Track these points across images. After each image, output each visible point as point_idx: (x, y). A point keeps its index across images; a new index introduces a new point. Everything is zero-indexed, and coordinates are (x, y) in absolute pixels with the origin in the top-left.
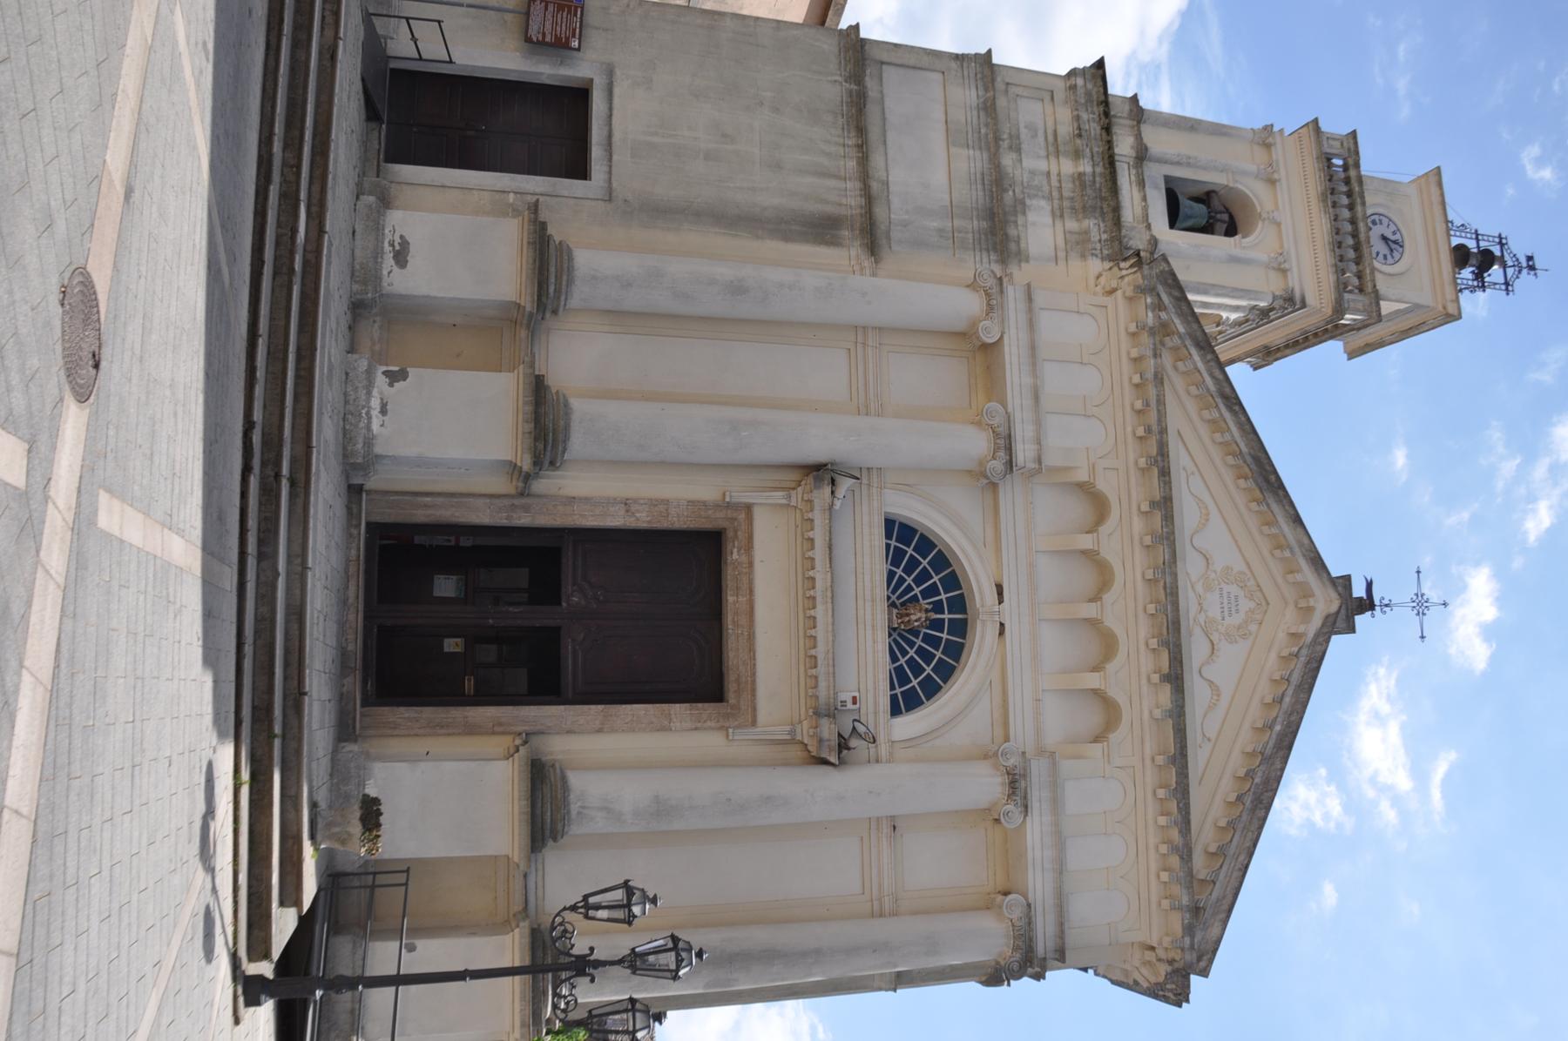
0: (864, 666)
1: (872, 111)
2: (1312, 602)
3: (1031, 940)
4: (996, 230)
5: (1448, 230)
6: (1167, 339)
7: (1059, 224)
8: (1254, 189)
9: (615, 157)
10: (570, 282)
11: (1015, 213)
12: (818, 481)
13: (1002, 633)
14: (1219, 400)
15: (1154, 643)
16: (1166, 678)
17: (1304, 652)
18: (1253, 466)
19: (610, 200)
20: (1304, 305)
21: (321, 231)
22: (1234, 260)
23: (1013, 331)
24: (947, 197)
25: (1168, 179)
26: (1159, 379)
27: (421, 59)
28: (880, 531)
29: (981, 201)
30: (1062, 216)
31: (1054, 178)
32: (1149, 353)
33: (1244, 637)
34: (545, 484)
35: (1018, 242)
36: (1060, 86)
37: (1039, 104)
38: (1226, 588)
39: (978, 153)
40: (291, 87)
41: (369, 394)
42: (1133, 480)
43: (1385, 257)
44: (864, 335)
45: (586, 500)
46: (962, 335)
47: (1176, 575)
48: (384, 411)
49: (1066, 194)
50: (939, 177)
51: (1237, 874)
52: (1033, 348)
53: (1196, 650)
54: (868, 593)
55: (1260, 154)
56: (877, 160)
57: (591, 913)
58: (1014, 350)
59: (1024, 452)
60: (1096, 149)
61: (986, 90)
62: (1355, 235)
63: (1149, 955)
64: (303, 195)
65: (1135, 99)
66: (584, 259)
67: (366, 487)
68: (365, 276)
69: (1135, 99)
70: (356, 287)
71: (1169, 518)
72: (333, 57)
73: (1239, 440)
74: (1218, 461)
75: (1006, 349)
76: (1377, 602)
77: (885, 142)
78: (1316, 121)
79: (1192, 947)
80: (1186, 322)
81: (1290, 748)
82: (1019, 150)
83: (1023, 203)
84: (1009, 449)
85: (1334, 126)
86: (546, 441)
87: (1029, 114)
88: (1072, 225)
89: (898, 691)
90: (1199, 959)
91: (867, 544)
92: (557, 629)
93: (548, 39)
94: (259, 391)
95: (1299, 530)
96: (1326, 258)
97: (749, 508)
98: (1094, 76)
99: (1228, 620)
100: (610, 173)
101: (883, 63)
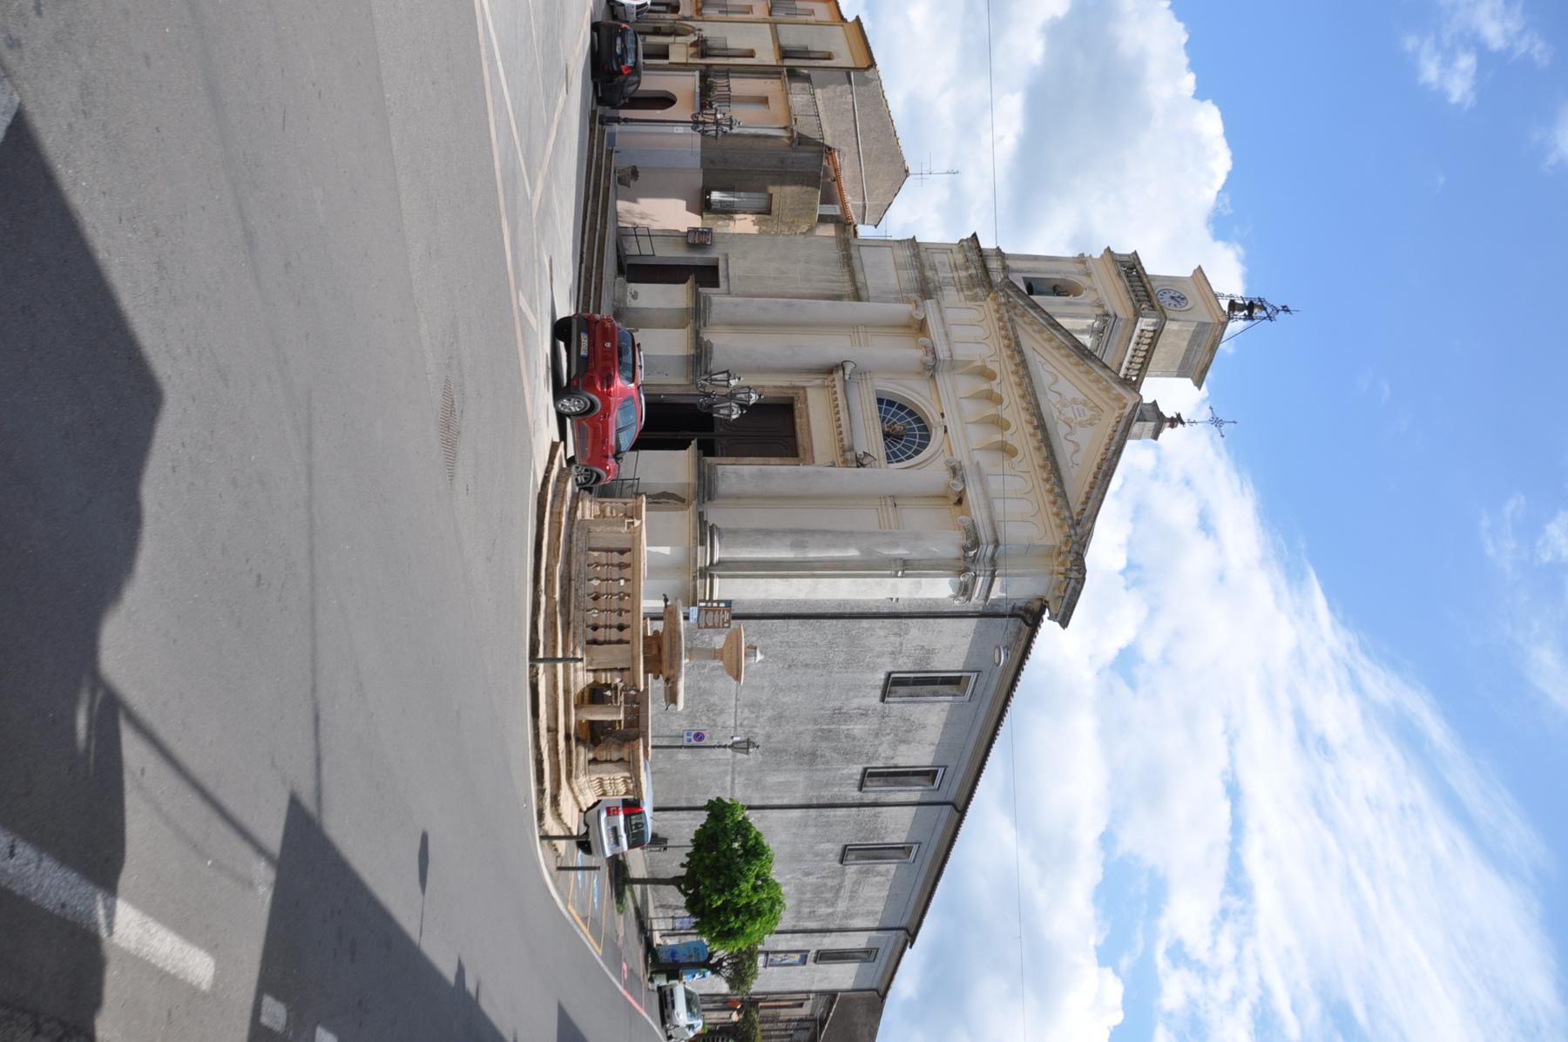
1: (856, 262)
8: (1083, 281)
16: (1047, 458)
22: (1070, 304)
26: (1011, 320)
28: (875, 405)
36: (955, 249)
44: (895, 500)
46: (907, 326)
50: (893, 281)
53: (1059, 431)
55: (1081, 267)
56: (860, 277)
59: (943, 354)
69: (1122, 573)
85: (1123, 248)
87: (938, 258)
96: (1124, 297)
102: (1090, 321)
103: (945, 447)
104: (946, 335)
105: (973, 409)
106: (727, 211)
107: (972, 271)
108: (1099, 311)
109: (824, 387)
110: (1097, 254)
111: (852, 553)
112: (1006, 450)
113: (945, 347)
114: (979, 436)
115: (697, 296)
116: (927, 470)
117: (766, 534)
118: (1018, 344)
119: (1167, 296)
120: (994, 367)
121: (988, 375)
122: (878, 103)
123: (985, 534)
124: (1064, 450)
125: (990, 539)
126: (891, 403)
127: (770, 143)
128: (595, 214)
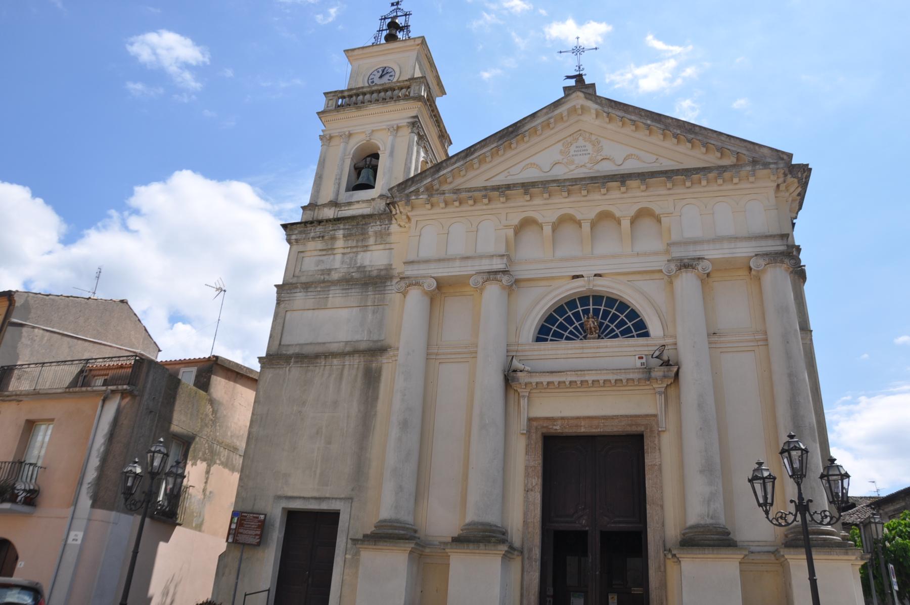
0: (621, 353)
1: (307, 350)
3: (776, 253)
4: (374, 282)
7: (370, 248)
8: (354, 144)
9: (327, 495)
10: (397, 521)
12: (515, 379)
13: (600, 275)
14: (468, 159)
19: (352, 499)
20: (416, 117)
22: (392, 154)
25: (348, 190)
26: (456, 191)
28: (542, 345)
30: (367, 246)
31: (346, 251)
32: (442, 197)
33: (599, 143)
36: (296, 248)
38: (572, 153)
39: (331, 292)
42: (512, 205)
45: (525, 514)
46: (432, 300)
49: (354, 244)
50: (344, 313)
51: (732, 141)
52: (440, 260)
53: (607, 168)
55: (334, 142)
56: (334, 348)
58: (441, 270)
59: (498, 264)
61: (296, 288)
66: (385, 513)
69: (304, 208)
71: (533, 184)
73: (490, 148)
75: (440, 275)
77: (324, 343)
78: (318, 113)
79: (775, 163)
80: (426, 177)
84: (496, 272)
86: (490, 536)
87: (310, 265)
88: (371, 241)
90: (783, 159)
93: (259, 533)
95: (539, 114)
97: (530, 420)
98: (291, 230)
100: (336, 499)
104: (467, 258)
107: (340, 234)
120: (515, 220)
122: (47, 301)
125: (779, 242)
127: (125, 421)
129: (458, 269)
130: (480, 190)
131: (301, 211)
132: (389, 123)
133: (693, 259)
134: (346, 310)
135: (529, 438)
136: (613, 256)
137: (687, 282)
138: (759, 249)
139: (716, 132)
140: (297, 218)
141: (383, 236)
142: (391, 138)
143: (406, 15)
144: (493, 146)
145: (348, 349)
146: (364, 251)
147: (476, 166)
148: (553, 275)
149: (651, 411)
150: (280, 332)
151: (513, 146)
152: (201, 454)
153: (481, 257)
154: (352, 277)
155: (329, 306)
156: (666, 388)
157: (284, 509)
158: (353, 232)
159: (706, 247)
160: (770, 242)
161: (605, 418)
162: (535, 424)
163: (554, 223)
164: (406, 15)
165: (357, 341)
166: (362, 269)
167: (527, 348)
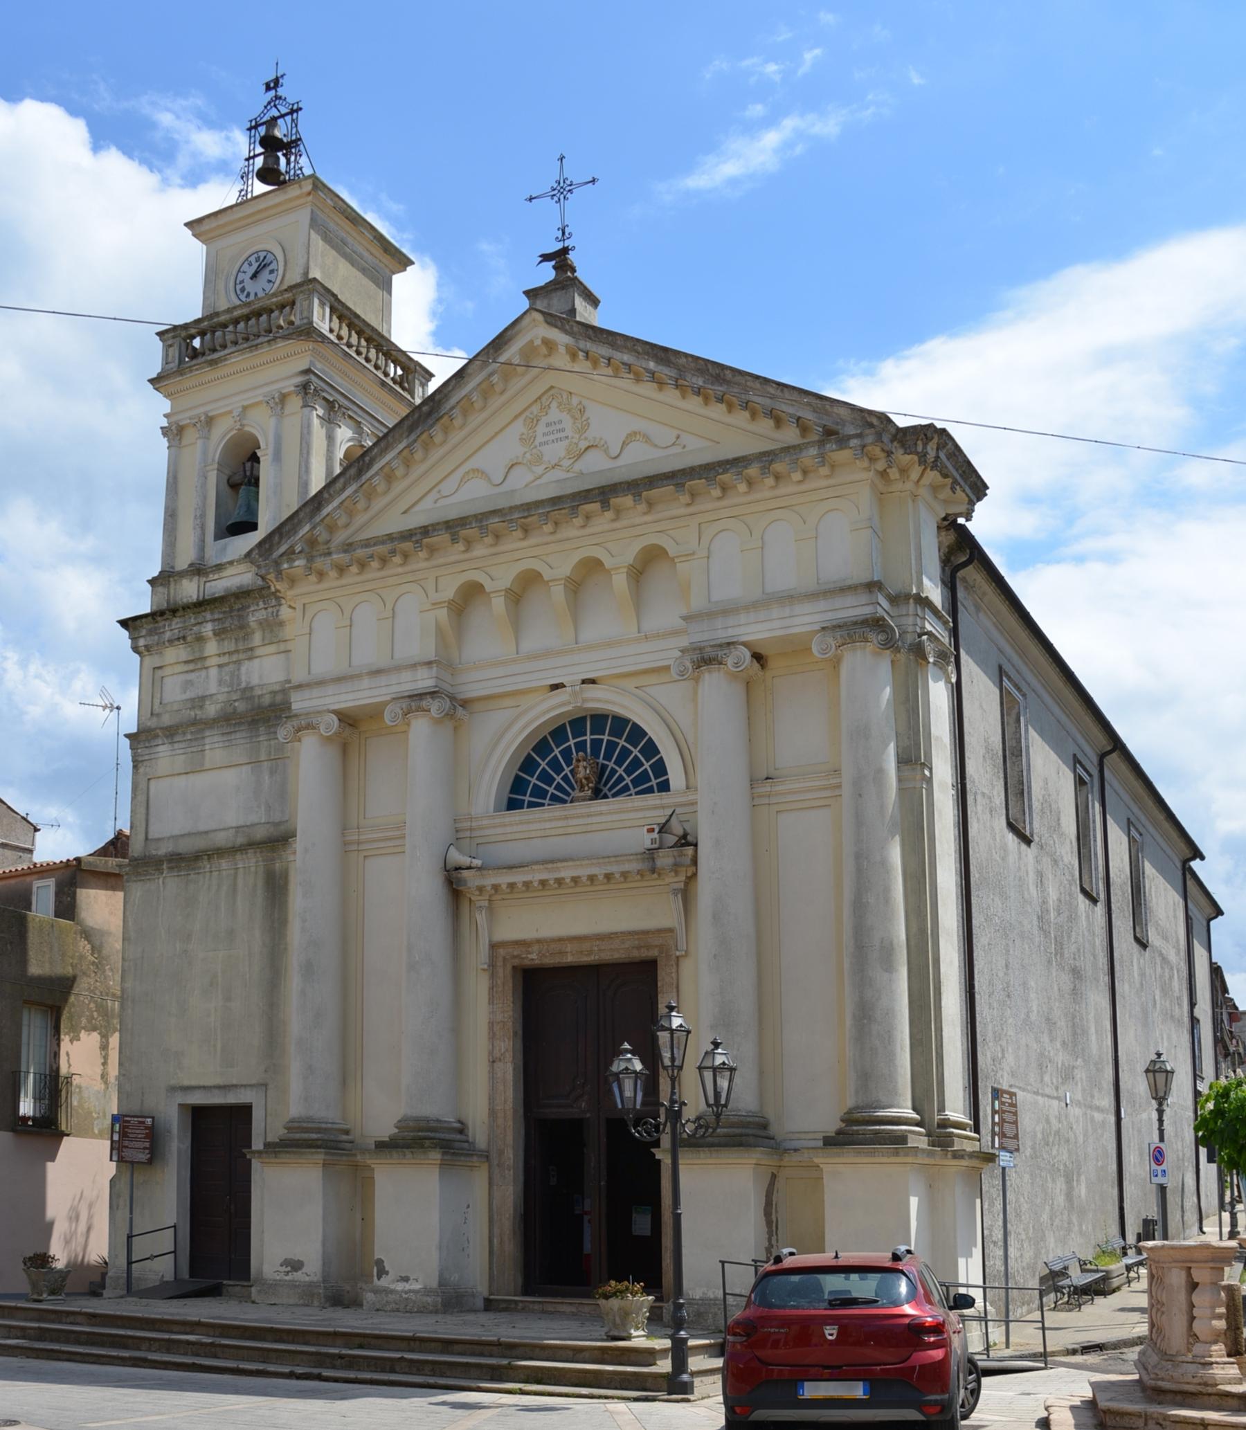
0: (623, 823)
1: (185, 847)
2: (538, 342)
3: (855, 623)
4: (263, 716)
5: (248, 201)
6: (320, 539)
7: (258, 652)
8: (222, 432)
9: (235, 1082)
10: (310, 1119)
11: (252, 698)
12: (460, 881)
13: (593, 681)
14: (364, 478)
15: (578, 521)
16: (637, 496)
17: (582, 344)
18: (418, 431)
19: (266, 1085)
20: (308, 371)
21: (199, 1324)
22: (277, 457)
23: (327, 700)
24: (245, 768)
25: (218, 537)
26: (348, 547)
27: (174, 1252)
28: (516, 815)
29: (244, 734)
30: (251, 649)
31: (225, 659)
32: (328, 560)
33: (582, 411)
34: (479, 1135)
35: (274, 693)
36: (152, 661)
37: (166, 680)
38: (540, 439)
39: (207, 741)
40: (102, 1345)
41: (392, 1292)
42: (441, 561)
43: (272, 272)
44: (761, 780)
45: (491, 1099)
46: (345, 749)
47: (511, 508)
48: (406, 1279)
49: (232, 647)
51: (787, 394)
52: (339, 680)
53: (596, 468)
54: (560, 824)
55: (190, 436)
56: (221, 839)
57: (723, 1102)
58: (343, 697)
59: (424, 680)
60: (193, 621)
61: (157, 736)
62: (247, 318)
63: (894, 473)
64: (166, 1336)
65: (152, 582)
66: (295, 1109)
67: (486, 1294)
68: (307, 1294)
69: (152, 582)
70: (316, 1303)
71: (463, 522)
72: (94, 1316)
73: (396, 451)
74: (442, 451)
75: (343, 706)
76: (559, 246)
77: (206, 833)
78: (151, 381)
79: (859, 436)
80: (299, 525)
81: (665, 349)
82: (203, 698)
83: (245, 690)
84: (421, 696)
85: (154, 358)
86: (425, 1138)
87: (174, 691)
88: (257, 638)
89: (633, 791)
90: (871, 425)
91: (520, 828)
92: (608, 1121)
93: (147, 1145)
94: (271, 1368)
95: (469, 371)
96: (265, 353)
97: (493, 946)
98: (135, 629)
99: (569, 432)
100: (245, 1086)
101: (147, 839)
102: (316, 421)
103: (630, 684)
104: (378, 672)
105: (543, 631)
106: (54, 1087)
107: (208, 629)
108: (295, 402)
109: (491, 910)
110: (164, 405)
111: (895, 854)
112: (649, 561)
113: (406, 676)
114: (606, 620)
115: (276, 1148)
116: (696, 726)
117: (866, 1017)
118: (407, 536)
119: (251, 286)
120: (449, 589)
121: (471, 593)
123: (855, 608)
124: (639, 459)
125: (864, 598)
126: (518, 785)
128: (170, 1346)
129: (367, 693)
130: (383, 543)
131: (149, 587)
132: (267, 389)
133: (720, 646)
134: (232, 771)
135: (493, 976)
136: (609, 644)
137: (716, 689)
138: (830, 616)
139: (758, 377)
140: (144, 607)
141: (273, 626)
142: (272, 422)
143: (292, 112)
144: (401, 446)
145: (241, 840)
146: (250, 659)
147: (380, 489)
148: (509, 689)
149: (666, 923)
150: (143, 817)
151: (438, 438)
152: (84, 1021)
153: (398, 669)
154: (235, 708)
155: (207, 766)
156: (686, 884)
157: (182, 1106)
158: (227, 624)
159: (743, 618)
160: (850, 600)
161: (600, 937)
162: (502, 951)
163: (508, 591)
164: (292, 112)
165: (253, 825)
166: (248, 694)
167: (485, 822)
